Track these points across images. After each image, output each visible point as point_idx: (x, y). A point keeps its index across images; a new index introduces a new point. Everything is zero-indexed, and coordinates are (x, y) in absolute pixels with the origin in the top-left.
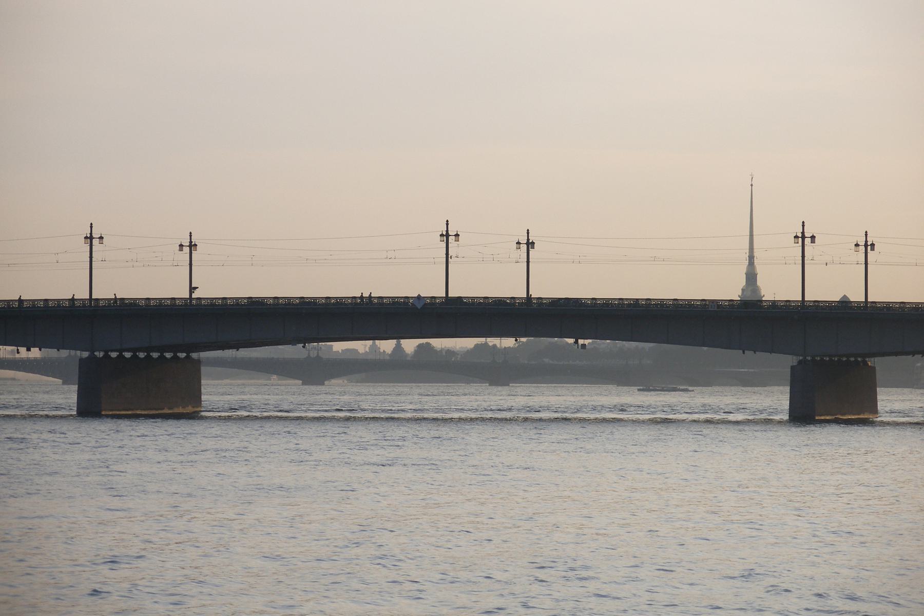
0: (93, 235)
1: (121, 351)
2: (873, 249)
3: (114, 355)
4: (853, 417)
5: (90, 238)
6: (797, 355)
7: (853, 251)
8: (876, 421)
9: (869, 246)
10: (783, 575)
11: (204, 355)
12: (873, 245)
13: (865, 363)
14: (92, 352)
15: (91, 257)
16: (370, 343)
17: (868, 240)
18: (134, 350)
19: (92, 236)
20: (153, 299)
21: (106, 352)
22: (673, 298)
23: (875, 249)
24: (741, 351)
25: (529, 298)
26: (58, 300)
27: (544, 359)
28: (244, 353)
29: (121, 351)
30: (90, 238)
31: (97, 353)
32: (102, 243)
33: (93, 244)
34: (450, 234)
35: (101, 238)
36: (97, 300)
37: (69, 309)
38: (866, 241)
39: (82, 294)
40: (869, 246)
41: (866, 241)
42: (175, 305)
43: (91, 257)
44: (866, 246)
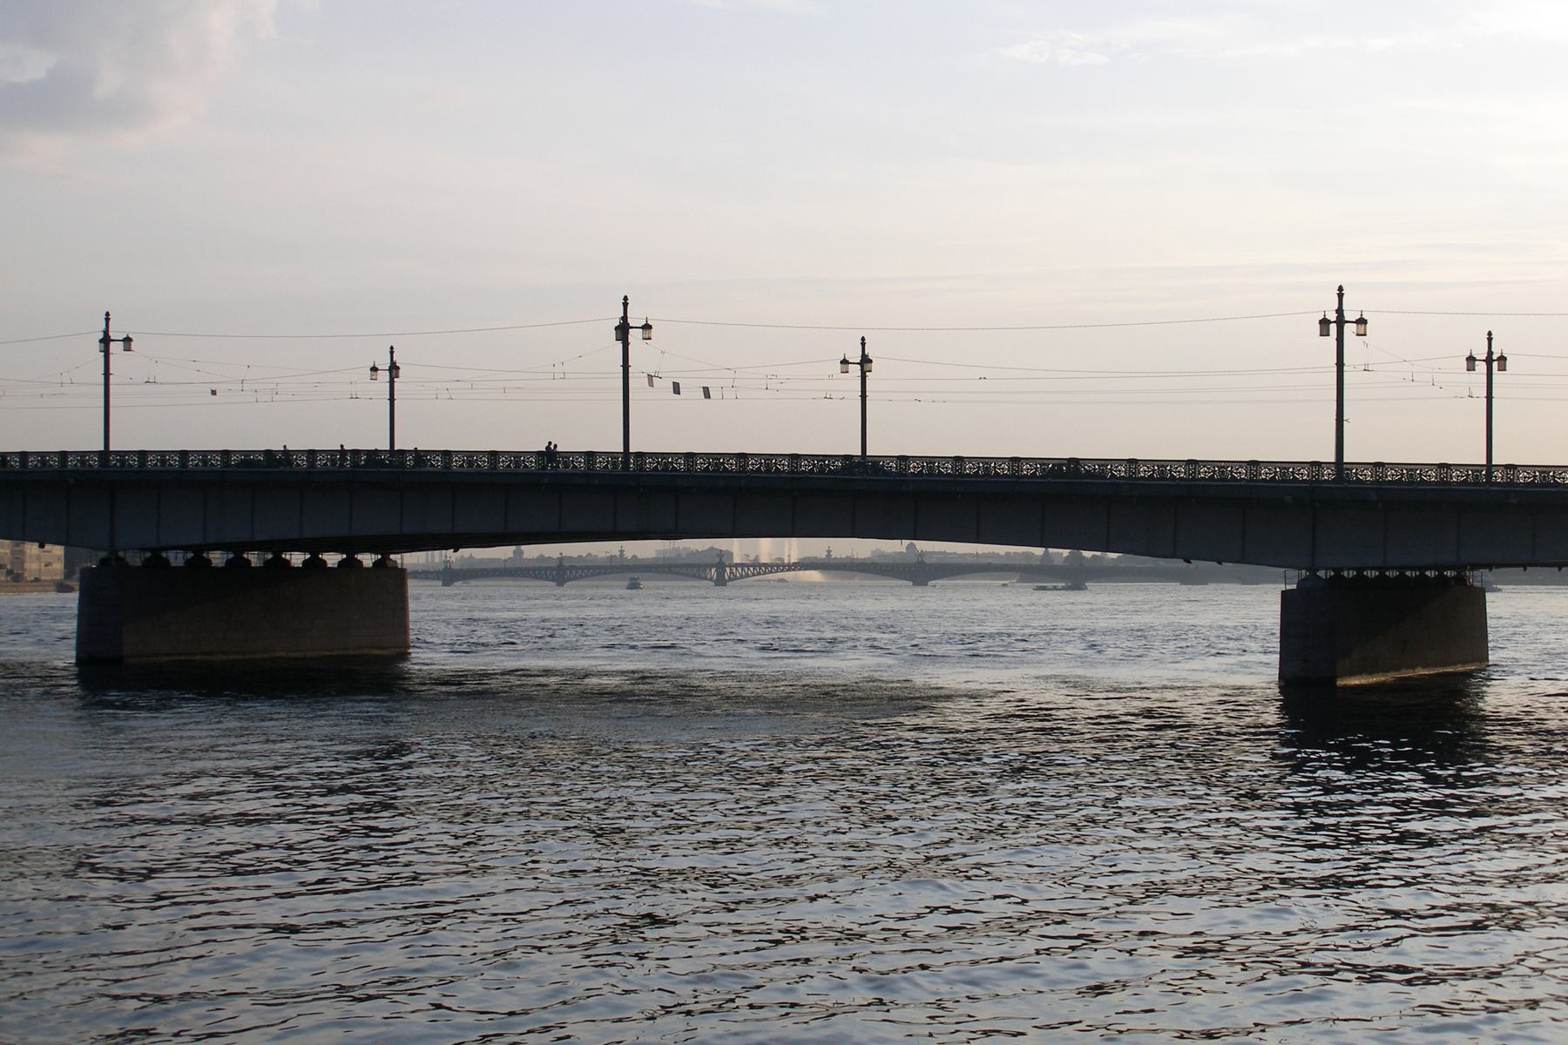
0: (110, 334)
1: (239, 548)
2: (1502, 368)
3: (217, 558)
4: (1363, 681)
5: (1335, 324)
6: (1299, 569)
7: (368, 380)
8: (1472, 693)
9: (1495, 362)
10: (700, 918)
11: (410, 560)
12: (1502, 359)
13: (1460, 580)
14: (1313, 570)
15: (107, 374)
16: (906, 542)
17: (1493, 350)
18: (1440, 568)
19: (108, 334)
20: (651, 455)
21: (1360, 570)
22: (1127, 458)
23: (1507, 368)
24: (1557, 569)
25: (105, 454)
26: (930, 460)
27: (192, 555)
28: (532, 551)
29: (1382, 569)
30: (1335, 324)
31: (1428, 573)
32: (650, 339)
33: (111, 351)
34: (112, 338)
35: (128, 340)
36: (640, 455)
37: (790, 476)
38: (1490, 353)
39: (373, 439)
40: (1495, 362)
41: (1490, 353)
42: (743, 469)
43: (107, 374)
44: (1489, 361)
